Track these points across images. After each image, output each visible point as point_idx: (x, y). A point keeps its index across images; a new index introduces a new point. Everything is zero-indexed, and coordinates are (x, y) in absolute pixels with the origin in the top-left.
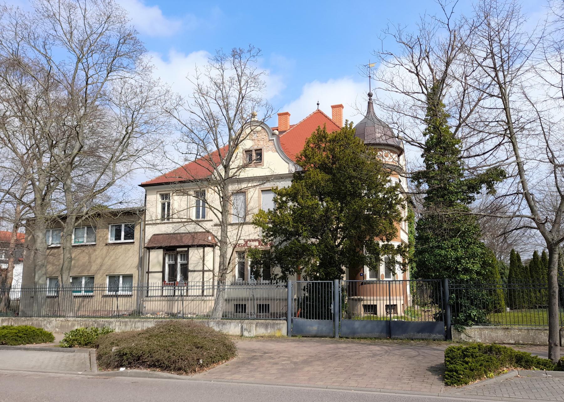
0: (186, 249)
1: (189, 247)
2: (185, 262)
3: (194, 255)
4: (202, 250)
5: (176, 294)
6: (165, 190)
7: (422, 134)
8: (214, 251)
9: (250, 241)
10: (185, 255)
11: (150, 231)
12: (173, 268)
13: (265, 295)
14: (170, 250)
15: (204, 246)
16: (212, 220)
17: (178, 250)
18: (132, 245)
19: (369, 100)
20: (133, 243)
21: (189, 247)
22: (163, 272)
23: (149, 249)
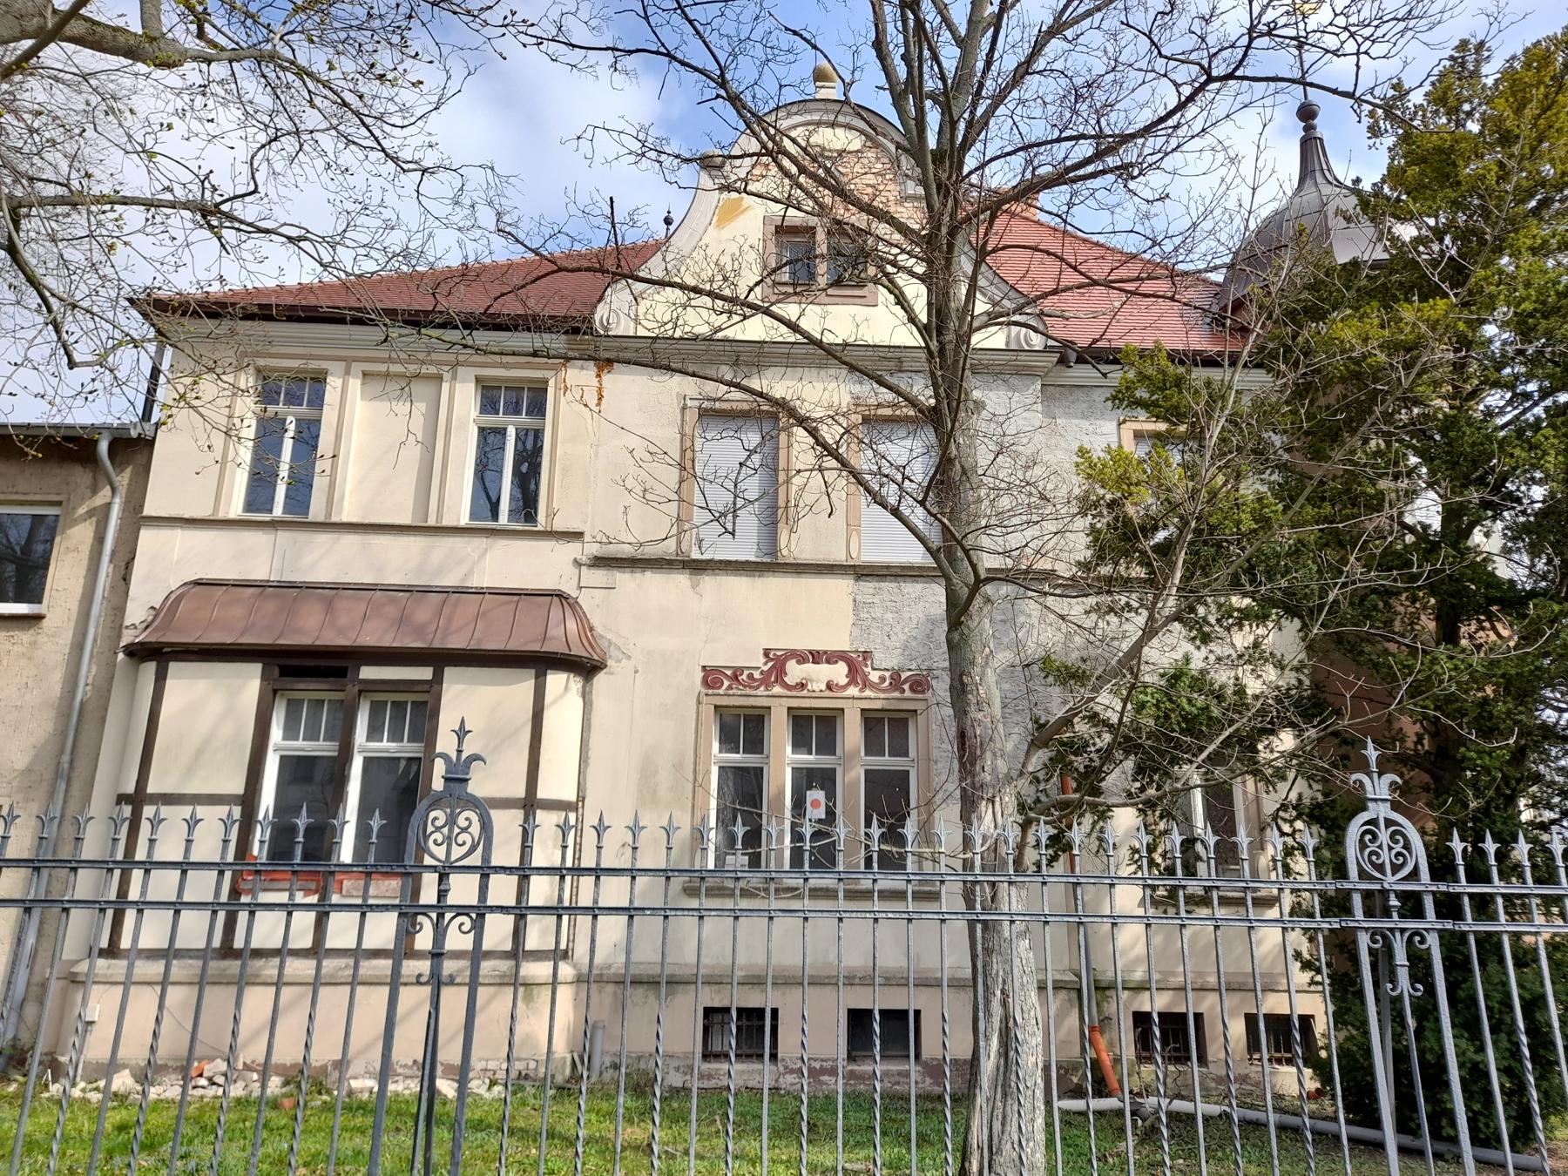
0: (425, 673)
1: (441, 659)
2: (403, 748)
3: (474, 706)
4: (530, 684)
5: (532, 942)
6: (292, 346)
7: (1087, 446)
8: (586, 695)
9: (802, 657)
10: (419, 711)
11: (165, 564)
12: (314, 781)
13: (891, 959)
14: (304, 670)
15: (541, 662)
16: (578, 535)
17: (368, 673)
18: (24, 636)
19: (1306, 129)
20: (39, 618)
21: (441, 659)
22: (249, 800)
23: (156, 654)
